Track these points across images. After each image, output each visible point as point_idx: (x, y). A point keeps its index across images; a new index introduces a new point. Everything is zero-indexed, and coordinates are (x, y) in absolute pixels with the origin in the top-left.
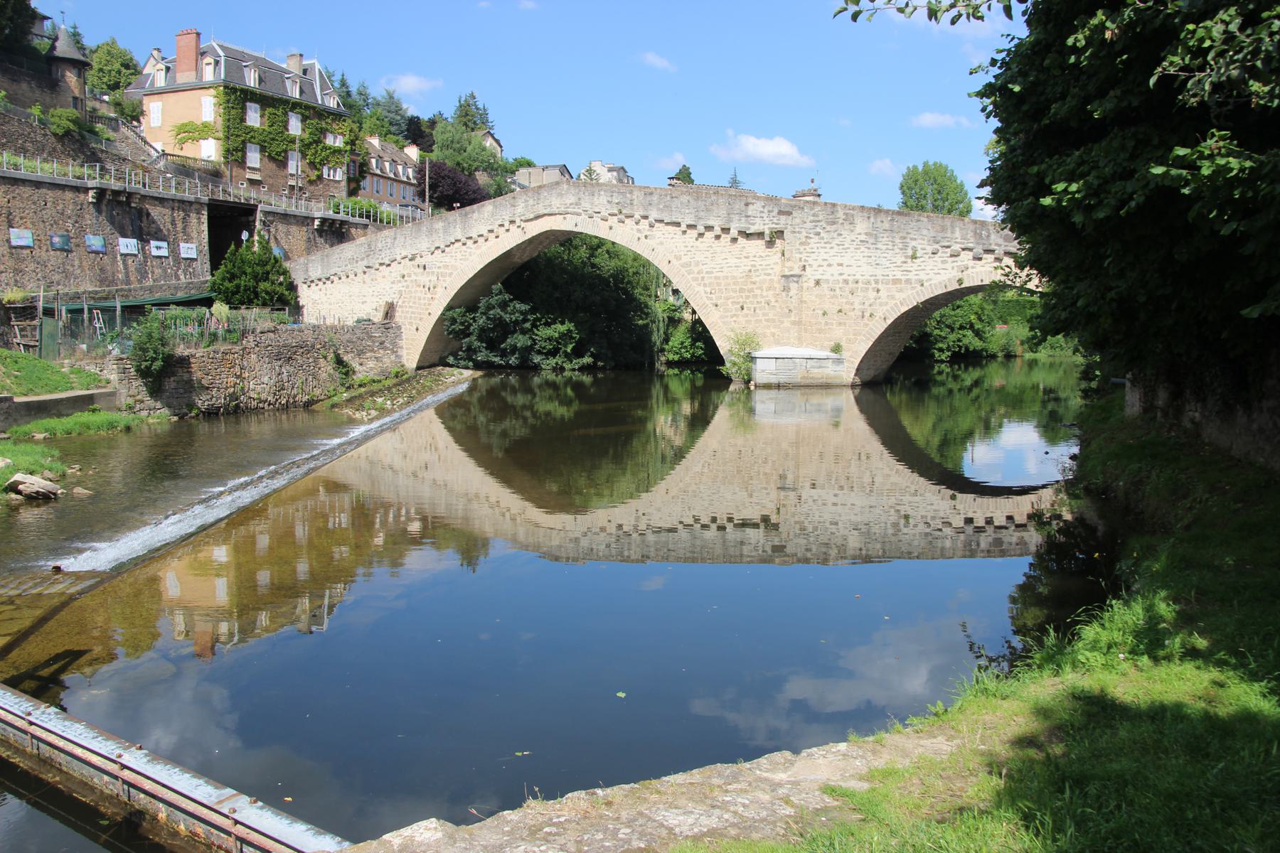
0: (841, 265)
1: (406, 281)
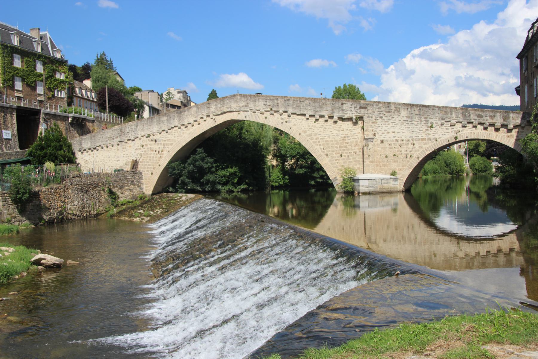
0: (394, 132)
1: (144, 148)
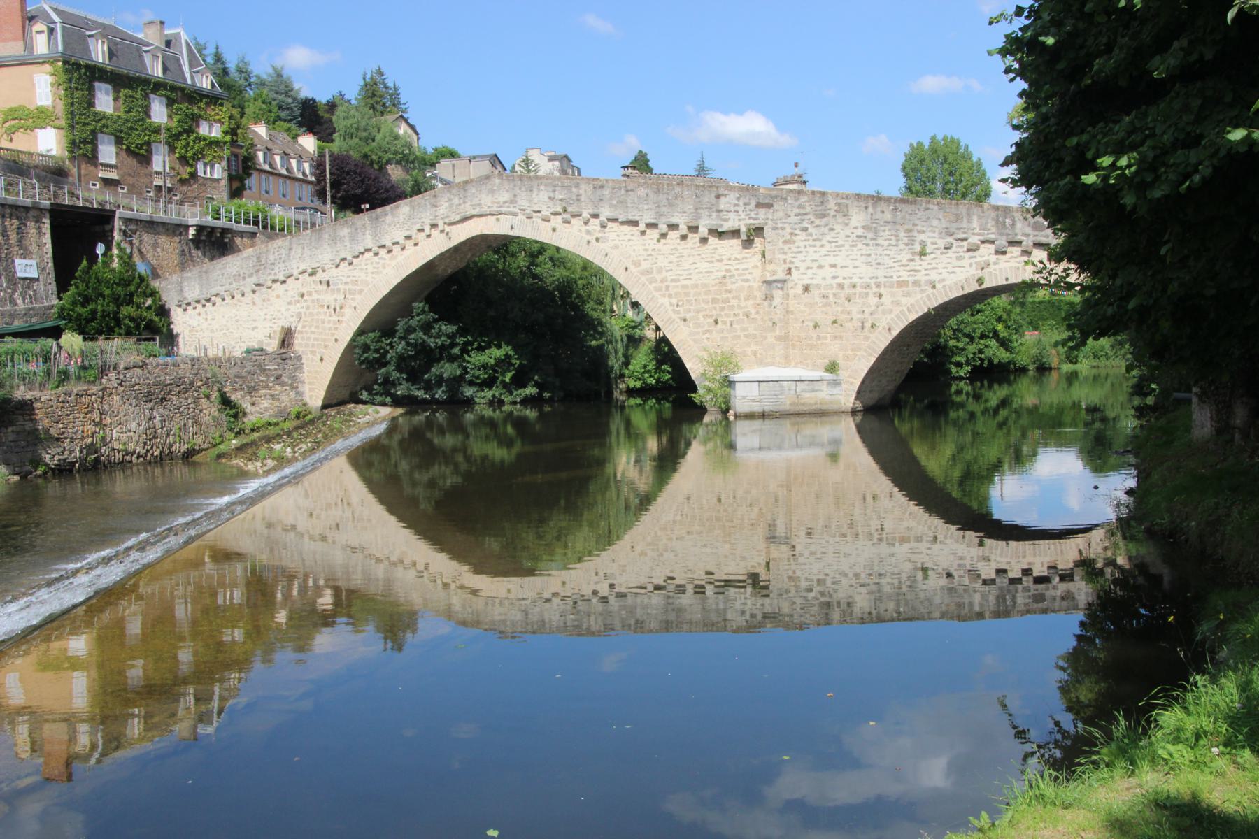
0: (834, 266)
1: (306, 301)
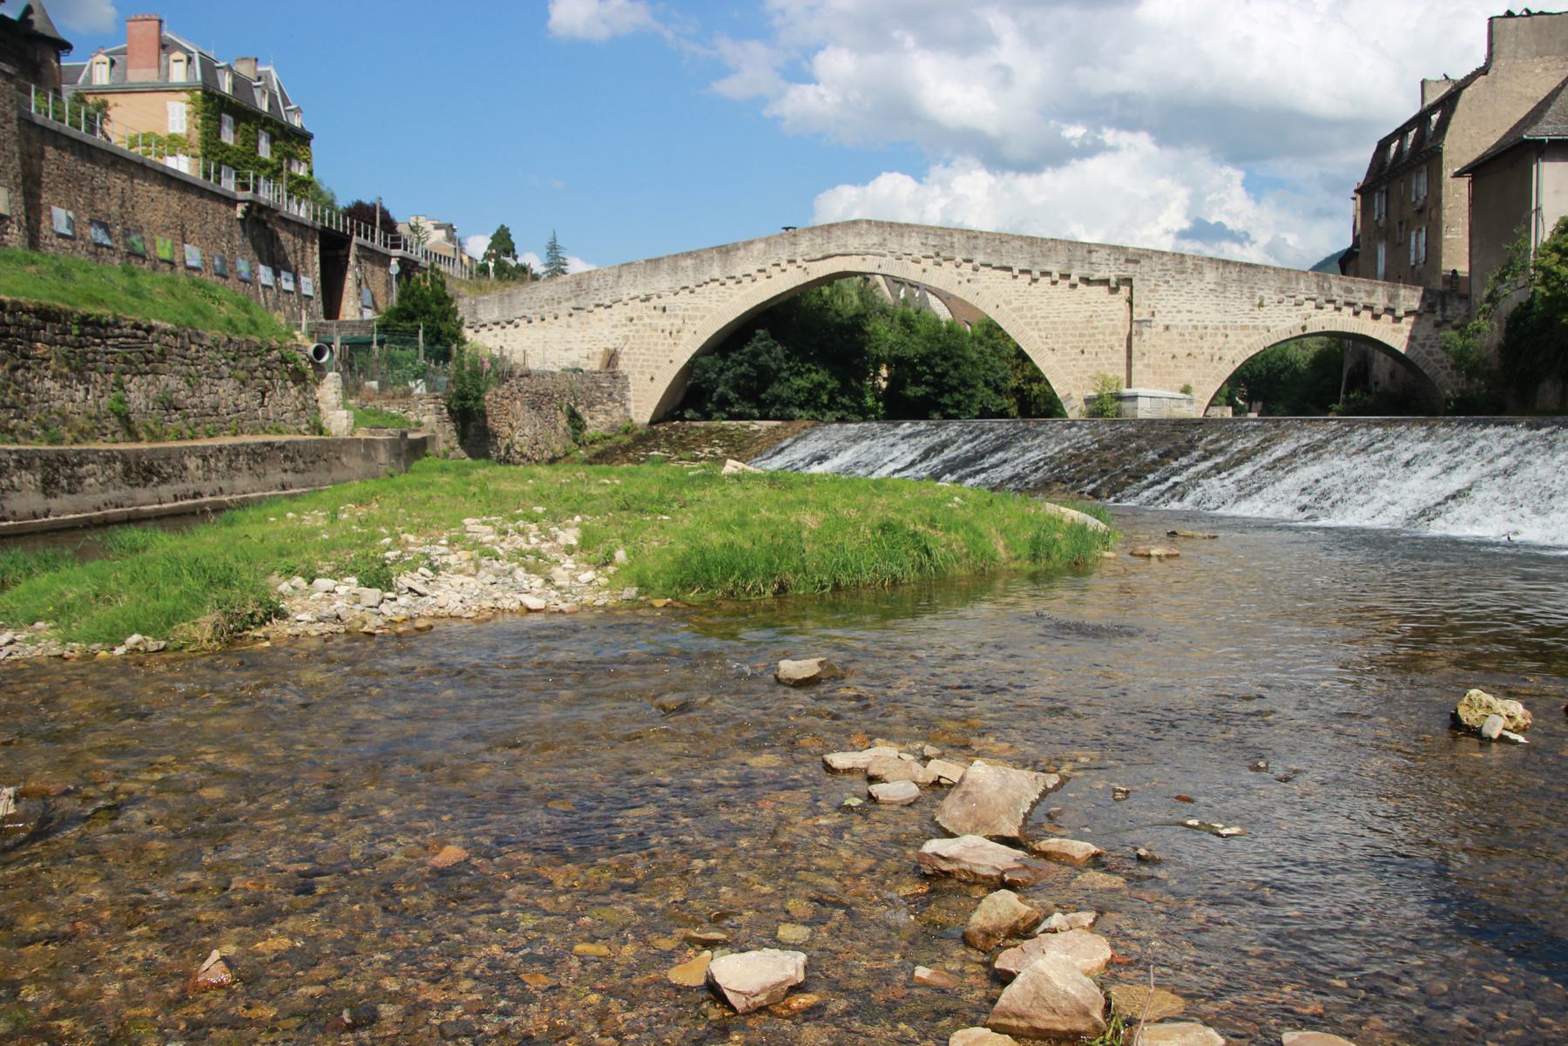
0: (1190, 311)
